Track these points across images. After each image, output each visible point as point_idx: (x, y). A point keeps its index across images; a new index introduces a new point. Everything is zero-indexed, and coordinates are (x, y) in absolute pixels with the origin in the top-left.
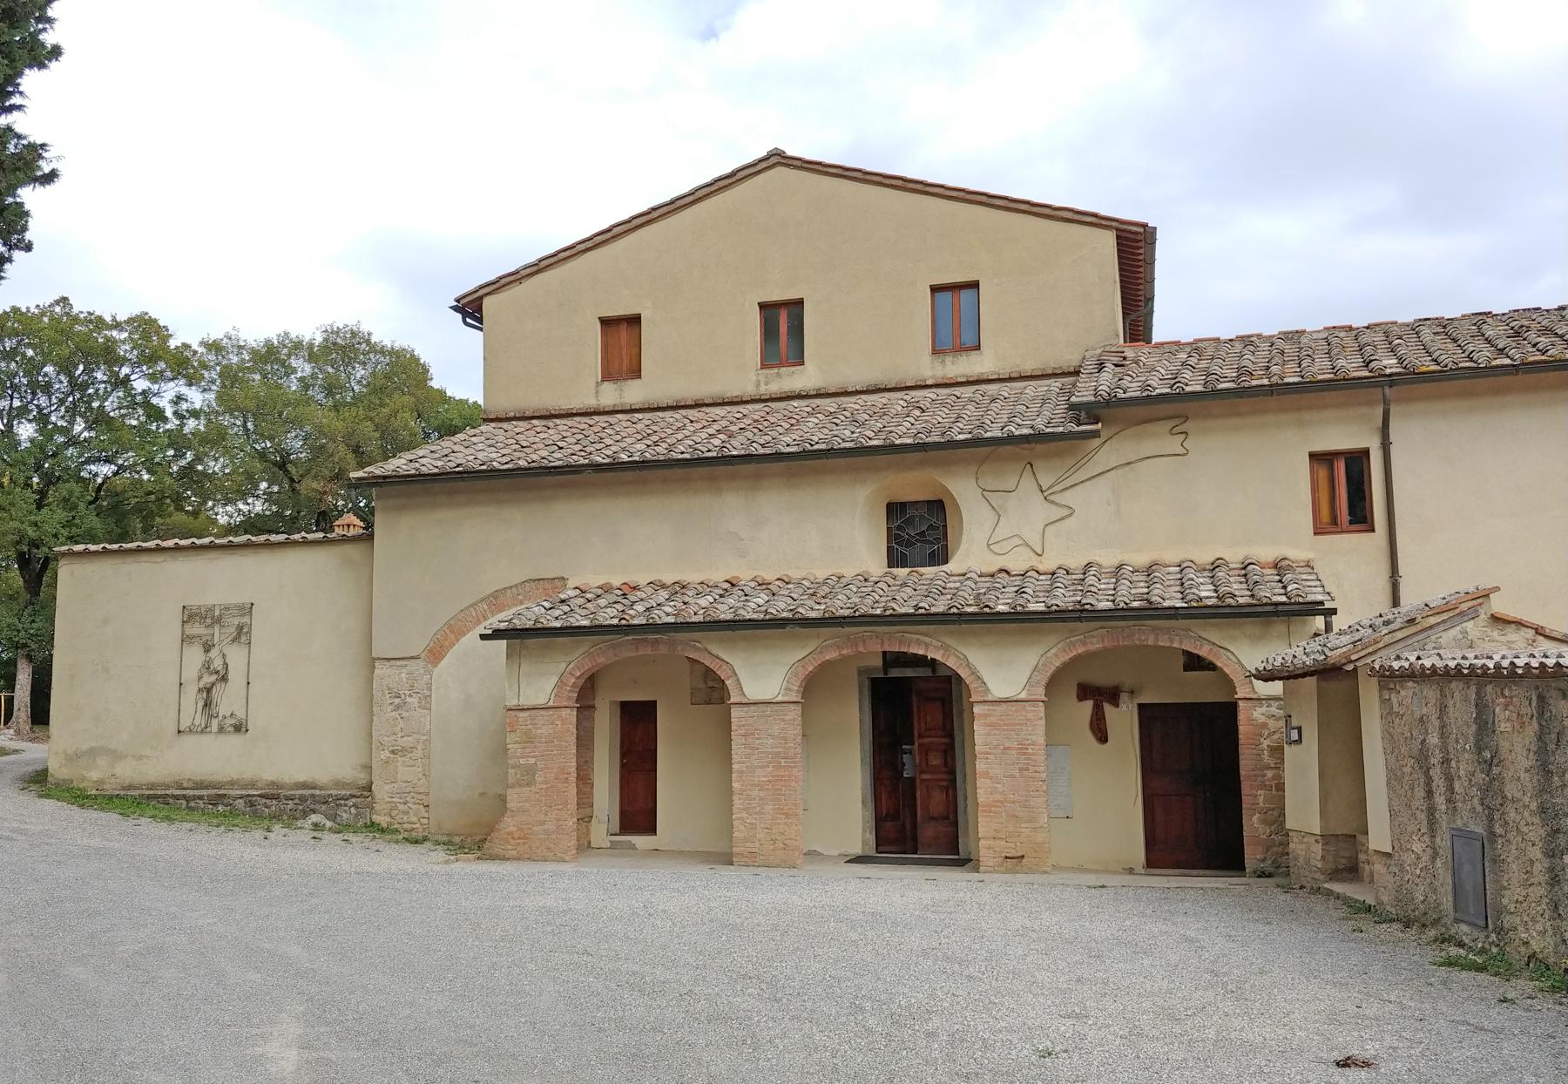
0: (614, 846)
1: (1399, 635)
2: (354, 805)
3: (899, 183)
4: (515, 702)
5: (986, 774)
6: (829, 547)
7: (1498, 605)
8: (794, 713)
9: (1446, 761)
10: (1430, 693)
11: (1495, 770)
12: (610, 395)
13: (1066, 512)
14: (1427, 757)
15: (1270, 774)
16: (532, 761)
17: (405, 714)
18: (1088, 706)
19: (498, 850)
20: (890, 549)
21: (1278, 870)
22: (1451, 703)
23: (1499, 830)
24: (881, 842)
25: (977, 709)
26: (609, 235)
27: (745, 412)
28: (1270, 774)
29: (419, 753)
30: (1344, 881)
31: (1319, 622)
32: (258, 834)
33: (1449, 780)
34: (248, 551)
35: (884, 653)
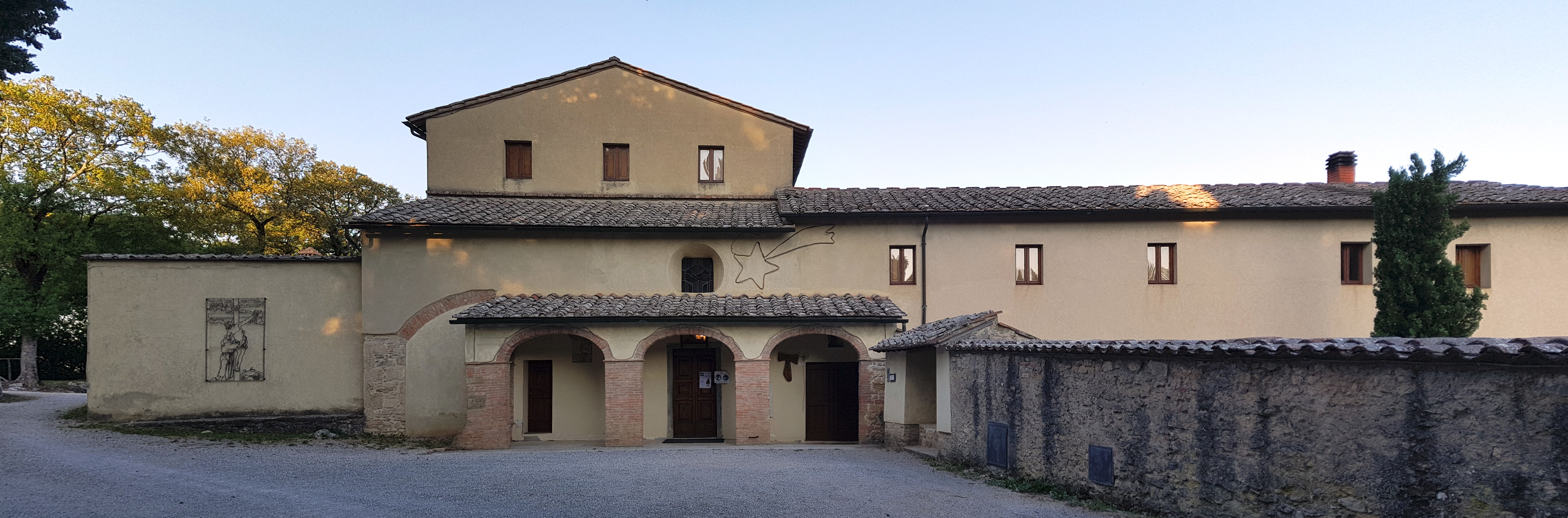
0: (526, 439)
1: (960, 331)
2: (351, 423)
3: (684, 87)
4: (472, 360)
5: (741, 397)
6: (650, 276)
7: (1001, 319)
8: (639, 366)
9: (988, 391)
10: (981, 359)
11: (1017, 396)
12: (511, 187)
13: (776, 268)
14: (977, 389)
15: (873, 396)
16: (483, 394)
17: (388, 368)
18: (783, 363)
19: (462, 445)
20: (683, 282)
21: (880, 440)
22: (993, 364)
23: (1017, 423)
24: (675, 435)
25: (737, 365)
26: (511, 92)
27: (515, 202)
28: (873, 396)
29: (398, 391)
30: (913, 445)
31: (899, 326)
32: (226, 441)
33: (989, 399)
34: (261, 265)
35: (682, 336)
